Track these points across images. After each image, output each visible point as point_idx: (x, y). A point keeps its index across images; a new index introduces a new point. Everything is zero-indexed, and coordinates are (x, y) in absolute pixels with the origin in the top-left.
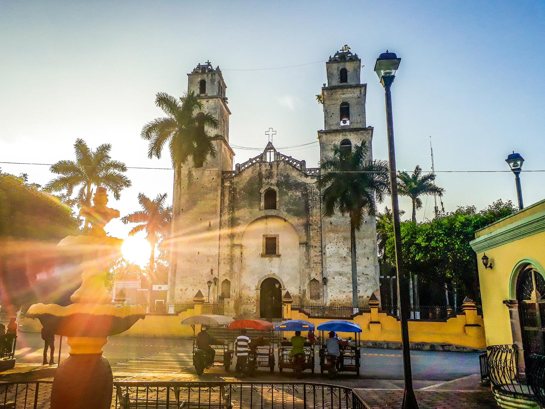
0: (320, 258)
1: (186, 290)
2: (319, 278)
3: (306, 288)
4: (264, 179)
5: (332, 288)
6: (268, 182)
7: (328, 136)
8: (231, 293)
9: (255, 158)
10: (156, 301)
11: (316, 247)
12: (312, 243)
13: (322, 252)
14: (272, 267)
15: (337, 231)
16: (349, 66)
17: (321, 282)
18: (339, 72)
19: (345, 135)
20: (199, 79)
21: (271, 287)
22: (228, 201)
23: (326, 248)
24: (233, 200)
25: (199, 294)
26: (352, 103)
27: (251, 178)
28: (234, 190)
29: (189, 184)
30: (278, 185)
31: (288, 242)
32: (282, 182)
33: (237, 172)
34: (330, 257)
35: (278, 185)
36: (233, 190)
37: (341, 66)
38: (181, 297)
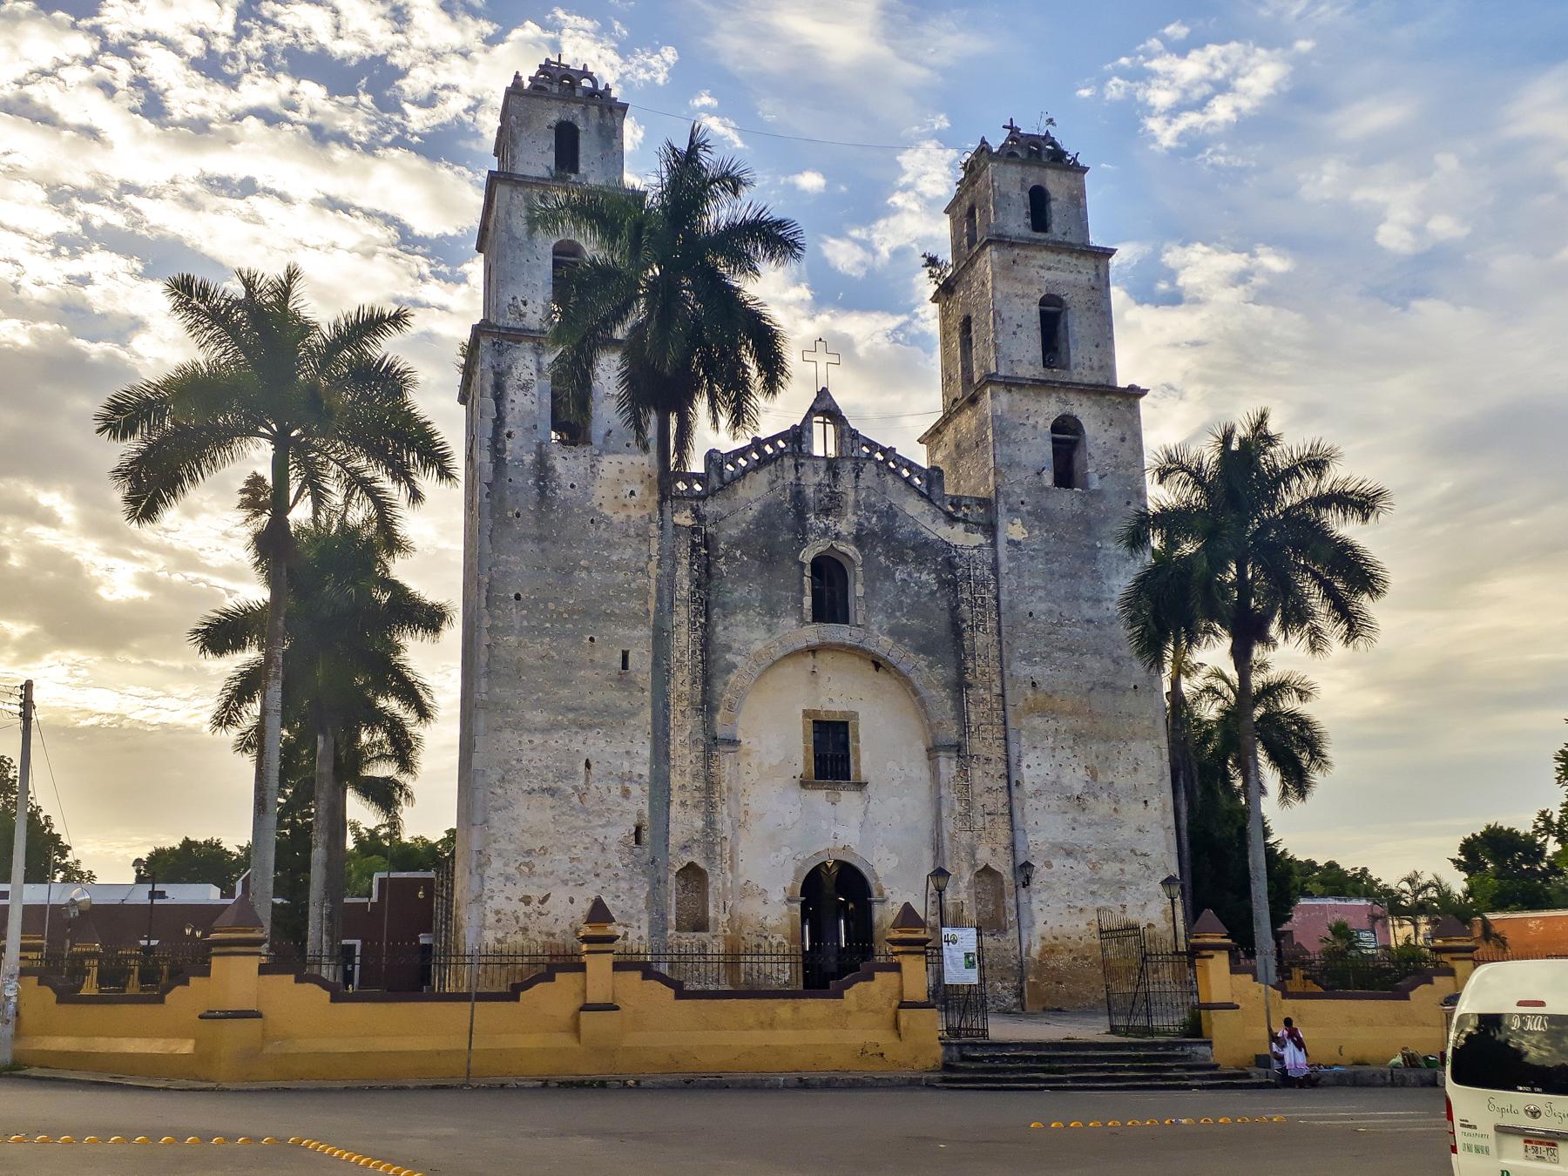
1: (542, 902)
2: (1003, 866)
3: (963, 896)
4: (811, 517)
5: (1044, 896)
6: (828, 528)
7: (1016, 395)
8: (711, 914)
9: (772, 441)
10: (358, 943)
11: (988, 760)
12: (976, 745)
13: (1008, 777)
16: (1054, 183)
17: (1008, 877)
18: (1027, 195)
19: (1066, 403)
20: (554, 117)
21: (834, 893)
22: (686, 584)
23: (1024, 765)
24: (705, 578)
25: (599, 912)
27: (767, 506)
28: (709, 541)
29: (540, 504)
30: (858, 540)
31: (886, 738)
33: (715, 481)
34: (1037, 793)
35: (858, 540)
36: (704, 546)
37: (1033, 177)
38: (525, 930)
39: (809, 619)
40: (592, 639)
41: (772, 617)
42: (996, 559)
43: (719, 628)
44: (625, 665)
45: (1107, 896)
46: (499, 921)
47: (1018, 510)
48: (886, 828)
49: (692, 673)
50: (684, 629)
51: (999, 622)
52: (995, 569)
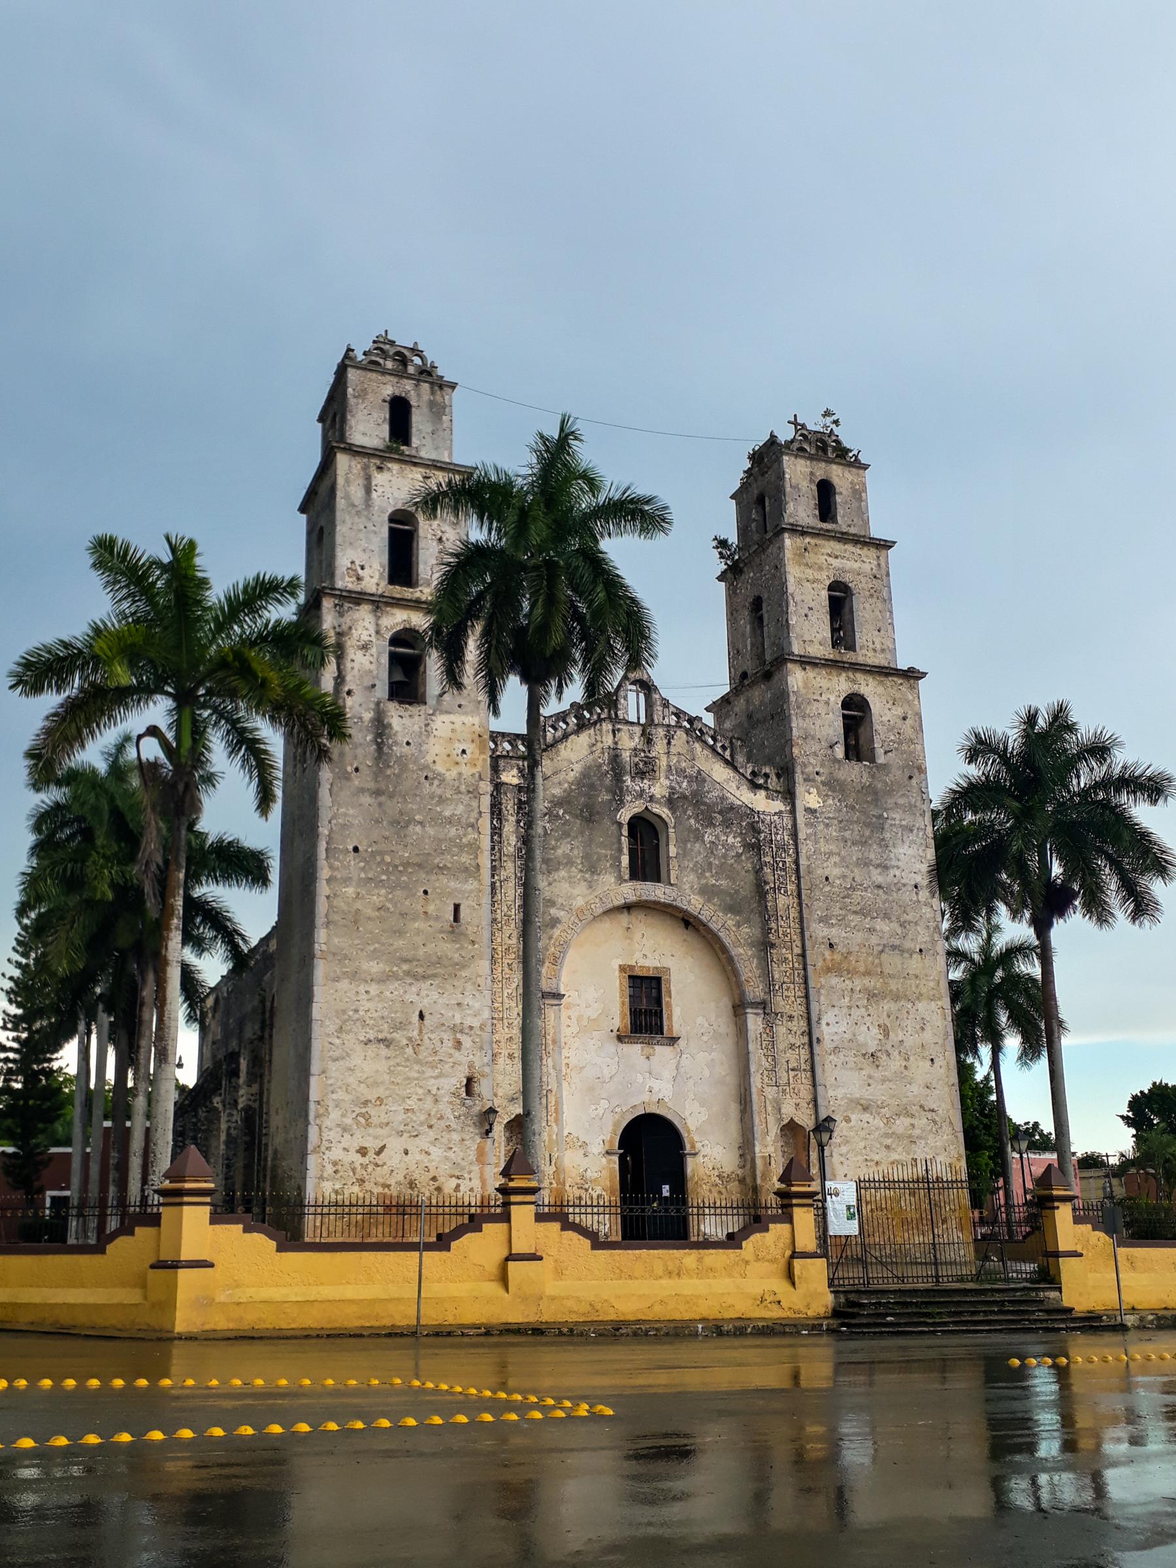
0: (804, 1054)
4: (627, 778)
5: (844, 1149)
6: (643, 791)
7: (811, 673)
10: (49, 1193)
11: (791, 1017)
19: (854, 682)
20: (388, 391)
23: (823, 1022)
26: (860, 586)
30: (671, 802)
31: (692, 998)
32: (684, 797)
34: (836, 1050)
39: (627, 877)
41: (593, 873)
44: (456, 918)
47: (814, 780)
52: (794, 835)
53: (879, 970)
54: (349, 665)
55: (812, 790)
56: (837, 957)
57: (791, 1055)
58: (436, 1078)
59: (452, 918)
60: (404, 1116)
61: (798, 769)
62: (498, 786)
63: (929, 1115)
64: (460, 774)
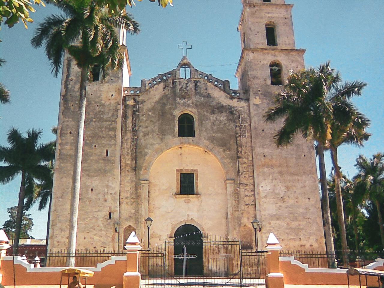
11: (247, 185)
14: (188, 211)
15: (272, 166)
21: (188, 237)
22: (131, 125)
34: (265, 197)
39: (177, 135)
40: (95, 146)
41: (163, 135)
42: (249, 111)
43: (142, 140)
44: (107, 155)
45: (294, 234)
46: (58, 245)
47: (258, 94)
48: (207, 213)
49: (132, 156)
50: (129, 141)
51: (251, 134)
52: (249, 114)
53: (285, 165)
54: (72, 70)
55: (257, 97)
56: (267, 161)
57: (246, 199)
58: (96, 212)
59: (105, 154)
60: (84, 225)
61: (251, 90)
62: (126, 107)
63: (307, 220)
64: (110, 103)
